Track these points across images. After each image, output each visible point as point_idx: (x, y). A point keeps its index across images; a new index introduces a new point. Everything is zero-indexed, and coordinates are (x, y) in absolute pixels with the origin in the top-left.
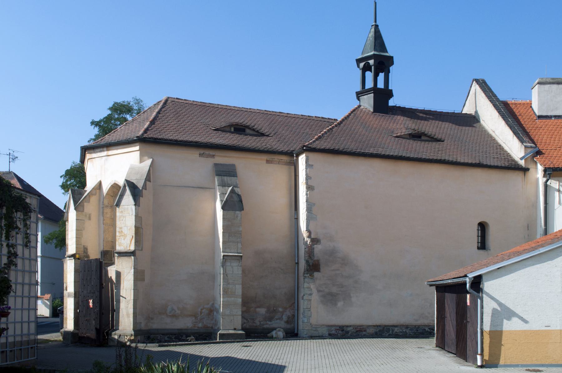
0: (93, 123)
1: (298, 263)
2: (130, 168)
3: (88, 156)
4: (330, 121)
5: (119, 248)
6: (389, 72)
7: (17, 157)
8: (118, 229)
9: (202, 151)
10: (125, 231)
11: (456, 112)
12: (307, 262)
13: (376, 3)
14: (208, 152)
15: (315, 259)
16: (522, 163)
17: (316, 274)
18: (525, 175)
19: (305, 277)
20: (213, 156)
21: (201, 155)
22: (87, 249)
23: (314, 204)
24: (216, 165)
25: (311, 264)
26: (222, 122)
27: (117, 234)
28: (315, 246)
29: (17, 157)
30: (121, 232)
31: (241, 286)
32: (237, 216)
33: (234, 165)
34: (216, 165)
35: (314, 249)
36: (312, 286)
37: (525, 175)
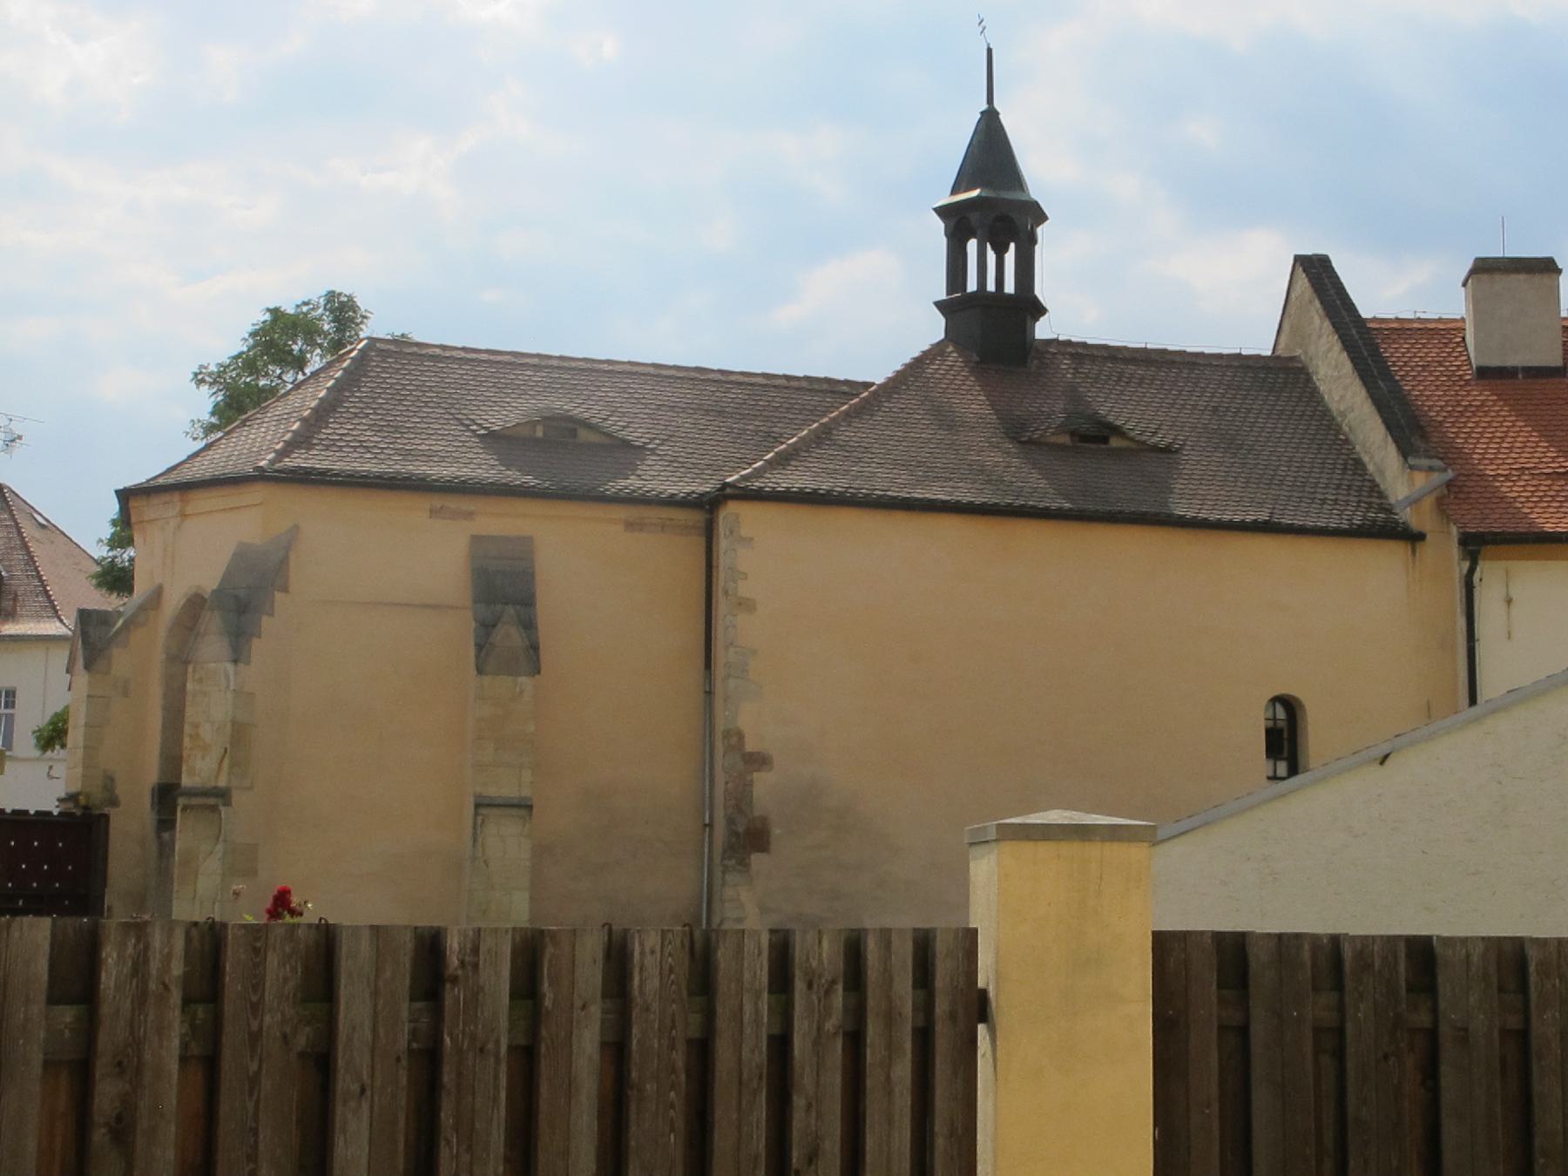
0: (199, 379)
1: (710, 825)
2: (235, 554)
3: (132, 504)
4: (854, 387)
5: (186, 781)
6: (1032, 240)
7: (20, 437)
8: (187, 729)
9: (437, 501)
10: (207, 733)
11: (1244, 352)
12: (731, 821)
13: (990, 51)
14: (453, 503)
15: (757, 813)
16: (1407, 516)
17: (757, 860)
18: (1414, 552)
19: (725, 870)
20: (469, 515)
21: (434, 513)
22: (112, 779)
23: (754, 652)
24: (476, 540)
25: (741, 830)
26: (505, 415)
27: (187, 741)
28: (755, 775)
29: (20, 437)
30: (195, 737)
31: (526, 895)
32: (522, 692)
33: (526, 542)
34: (476, 540)
35: (751, 784)
36: (745, 895)
37: (1414, 552)
